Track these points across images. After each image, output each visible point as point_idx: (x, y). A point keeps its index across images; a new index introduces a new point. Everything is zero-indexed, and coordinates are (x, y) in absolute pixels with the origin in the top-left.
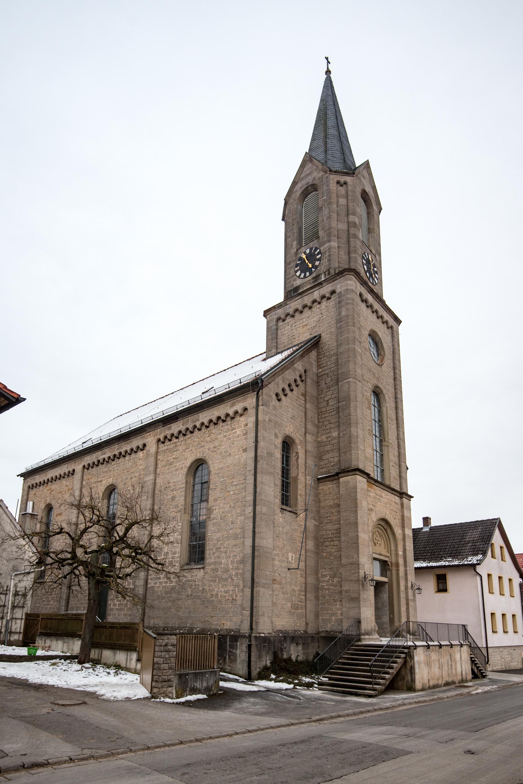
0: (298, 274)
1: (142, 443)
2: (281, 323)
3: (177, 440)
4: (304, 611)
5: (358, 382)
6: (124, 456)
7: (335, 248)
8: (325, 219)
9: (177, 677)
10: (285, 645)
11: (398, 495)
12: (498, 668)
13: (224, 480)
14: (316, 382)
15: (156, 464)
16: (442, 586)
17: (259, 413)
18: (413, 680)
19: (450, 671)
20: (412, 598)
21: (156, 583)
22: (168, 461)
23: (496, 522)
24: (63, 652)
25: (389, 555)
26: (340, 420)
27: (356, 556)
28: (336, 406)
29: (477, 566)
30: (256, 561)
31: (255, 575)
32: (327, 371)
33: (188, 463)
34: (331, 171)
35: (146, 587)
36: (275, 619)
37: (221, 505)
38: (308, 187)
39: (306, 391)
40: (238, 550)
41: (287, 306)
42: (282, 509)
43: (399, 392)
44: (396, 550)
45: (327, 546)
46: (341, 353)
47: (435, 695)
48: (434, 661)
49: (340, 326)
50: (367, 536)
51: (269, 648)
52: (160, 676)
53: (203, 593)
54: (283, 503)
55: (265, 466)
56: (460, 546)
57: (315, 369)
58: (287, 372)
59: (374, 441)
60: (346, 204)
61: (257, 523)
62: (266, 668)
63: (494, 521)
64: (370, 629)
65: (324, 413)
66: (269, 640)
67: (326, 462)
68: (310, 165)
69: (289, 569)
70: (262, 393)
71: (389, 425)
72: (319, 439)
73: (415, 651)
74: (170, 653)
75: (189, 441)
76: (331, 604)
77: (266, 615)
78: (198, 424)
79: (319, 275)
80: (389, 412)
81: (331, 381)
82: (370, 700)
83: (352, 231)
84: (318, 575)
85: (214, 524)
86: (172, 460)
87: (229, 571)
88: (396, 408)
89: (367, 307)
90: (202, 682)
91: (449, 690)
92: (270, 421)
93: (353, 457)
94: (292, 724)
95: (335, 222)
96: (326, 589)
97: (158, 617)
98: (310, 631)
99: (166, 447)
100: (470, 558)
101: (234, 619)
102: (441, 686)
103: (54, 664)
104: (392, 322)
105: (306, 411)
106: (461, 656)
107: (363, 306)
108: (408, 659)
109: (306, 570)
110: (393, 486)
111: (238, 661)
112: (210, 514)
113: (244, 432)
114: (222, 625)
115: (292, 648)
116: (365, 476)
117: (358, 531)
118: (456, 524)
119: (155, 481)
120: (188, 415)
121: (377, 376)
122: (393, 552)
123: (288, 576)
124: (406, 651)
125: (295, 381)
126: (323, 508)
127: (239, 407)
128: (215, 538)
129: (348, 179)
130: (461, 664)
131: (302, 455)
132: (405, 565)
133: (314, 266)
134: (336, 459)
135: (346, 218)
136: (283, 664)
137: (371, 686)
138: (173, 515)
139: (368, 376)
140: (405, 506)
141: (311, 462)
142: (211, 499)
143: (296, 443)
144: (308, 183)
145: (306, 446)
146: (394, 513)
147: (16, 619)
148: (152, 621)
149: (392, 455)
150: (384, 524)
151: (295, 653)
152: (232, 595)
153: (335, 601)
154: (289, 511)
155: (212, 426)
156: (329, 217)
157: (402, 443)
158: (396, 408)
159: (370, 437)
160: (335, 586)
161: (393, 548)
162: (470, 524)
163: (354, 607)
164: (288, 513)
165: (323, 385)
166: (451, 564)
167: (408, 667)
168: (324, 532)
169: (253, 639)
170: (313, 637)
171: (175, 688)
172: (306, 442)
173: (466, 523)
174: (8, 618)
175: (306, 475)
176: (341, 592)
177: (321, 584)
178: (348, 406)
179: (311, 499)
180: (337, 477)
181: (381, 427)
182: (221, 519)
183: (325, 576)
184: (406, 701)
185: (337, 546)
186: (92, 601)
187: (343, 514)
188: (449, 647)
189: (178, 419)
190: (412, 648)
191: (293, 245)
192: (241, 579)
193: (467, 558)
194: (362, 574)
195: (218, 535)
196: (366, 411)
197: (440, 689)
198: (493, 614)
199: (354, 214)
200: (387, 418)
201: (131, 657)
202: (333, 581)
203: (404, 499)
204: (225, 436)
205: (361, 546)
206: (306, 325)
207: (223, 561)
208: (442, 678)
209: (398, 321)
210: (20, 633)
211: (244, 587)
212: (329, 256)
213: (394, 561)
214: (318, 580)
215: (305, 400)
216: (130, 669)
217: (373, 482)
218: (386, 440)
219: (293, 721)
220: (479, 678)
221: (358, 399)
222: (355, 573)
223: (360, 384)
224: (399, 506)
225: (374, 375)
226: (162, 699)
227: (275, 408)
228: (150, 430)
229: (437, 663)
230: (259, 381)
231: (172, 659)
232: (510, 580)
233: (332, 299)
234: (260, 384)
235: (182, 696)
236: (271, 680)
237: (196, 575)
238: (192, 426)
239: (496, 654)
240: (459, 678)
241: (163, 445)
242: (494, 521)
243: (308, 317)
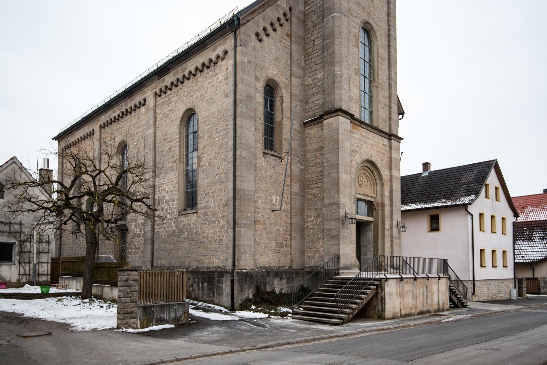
1: (143, 98)
3: (170, 92)
4: (289, 249)
5: (343, 16)
6: (130, 113)
9: (141, 310)
10: (268, 280)
11: (387, 137)
12: (485, 298)
14: (303, 21)
15: (155, 118)
16: (435, 227)
18: (383, 310)
19: (425, 301)
20: (397, 236)
21: (160, 228)
22: (164, 113)
23: (492, 164)
24: (77, 290)
25: (375, 196)
28: (321, 45)
29: (469, 206)
30: (237, 203)
31: (237, 217)
32: (313, 8)
35: (154, 232)
36: (258, 257)
39: (291, 31)
40: (223, 194)
42: (264, 153)
43: (392, 28)
44: (383, 191)
45: (312, 188)
47: (401, 323)
48: (408, 292)
50: (349, 176)
51: (251, 282)
53: (196, 235)
54: (266, 147)
55: (245, 110)
57: (301, 8)
58: (268, 9)
59: (362, 83)
61: (237, 167)
62: (248, 300)
63: (491, 163)
64: (349, 263)
65: (310, 54)
66: (252, 275)
70: (240, 32)
71: (380, 65)
72: (306, 82)
73: (386, 283)
74: (132, 288)
75: (180, 92)
77: (248, 253)
80: (380, 51)
82: (337, 328)
84: (304, 216)
85: (203, 171)
88: (389, 46)
90: (169, 313)
91: (420, 318)
92: (249, 62)
93: (336, 97)
94: (231, 352)
96: (310, 229)
98: (294, 267)
99: (162, 100)
100: (463, 199)
101: (221, 257)
102: (414, 315)
103: (59, 300)
105: (291, 52)
106: (438, 288)
108: (379, 290)
109: (291, 212)
110: (381, 127)
111: (224, 294)
115: (276, 282)
116: (349, 117)
117: (339, 172)
121: (367, 10)
122: (379, 193)
123: (272, 217)
124: (376, 283)
125: (279, 19)
126: (309, 152)
127: (219, 51)
128: (204, 184)
130: (438, 295)
132: (391, 205)
134: (321, 102)
137: (337, 315)
138: (171, 164)
139: (356, 10)
140: (393, 147)
142: (200, 147)
145: (291, 89)
146: (381, 155)
147: (42, 263)
148: (159, 261)
149: (382, 97)
150: (370, 166)
151: (279, 286)
152: (219, 236)
153: (318, 239)
154: (272, 155)
157: (393, 84)
158: (389, 46)
159: (357, 77)
160: (319, 226)
161: (379, 189)
164: (272, 157)
165: (310, 24)
167: (379, 297)
168: (310, 175)
169: (235, 275)
170: (297, 272)
171: (140, 319)
172: (291, 85)
173: (464, 166)
174: (35, 262)
176: (323, 231)
177: (306, 224)
178: (332, 43)
179: (295, 144)
180: (321, 120)
181: (371, 67)
183: (311, 217)
184: (384, 327)
185: (321, 187)
186: (89, 244)
187: (326, 156)
188: (426, 279)
189: (170, 70)
190: (383, 280)
193: (460, 199)
194: (342, 212)
196: (353, 49)
197: (412, 318)
198: (482, 251)
200: (378, 57)
204: (210, 83)
205: (341, 187)
207: (212, 205)
208: (416, 308)
210: (48, 275)
213: (379, 201)
214: (303, 220)
215: (291, 41)
217: (359, 123)
218: (376, 81)
219: (232, 349)
220: (459, 307)
221: (343, 36)
222: (336, 212)
223: (345, 19)
224: (387, 148)
225: (364, 10)
226: (125, 329)
227: (255, 49)
228: (149, 84)
229: (411, 294)
230: (235, 19)
231: (134, 293)
232: (503, 219)
234: (236, 22)
235: (148, 326)
237: (191, 220)
238: (181, 75)
239: (483, 286)
240: (436, 307)
242: (491, 163)
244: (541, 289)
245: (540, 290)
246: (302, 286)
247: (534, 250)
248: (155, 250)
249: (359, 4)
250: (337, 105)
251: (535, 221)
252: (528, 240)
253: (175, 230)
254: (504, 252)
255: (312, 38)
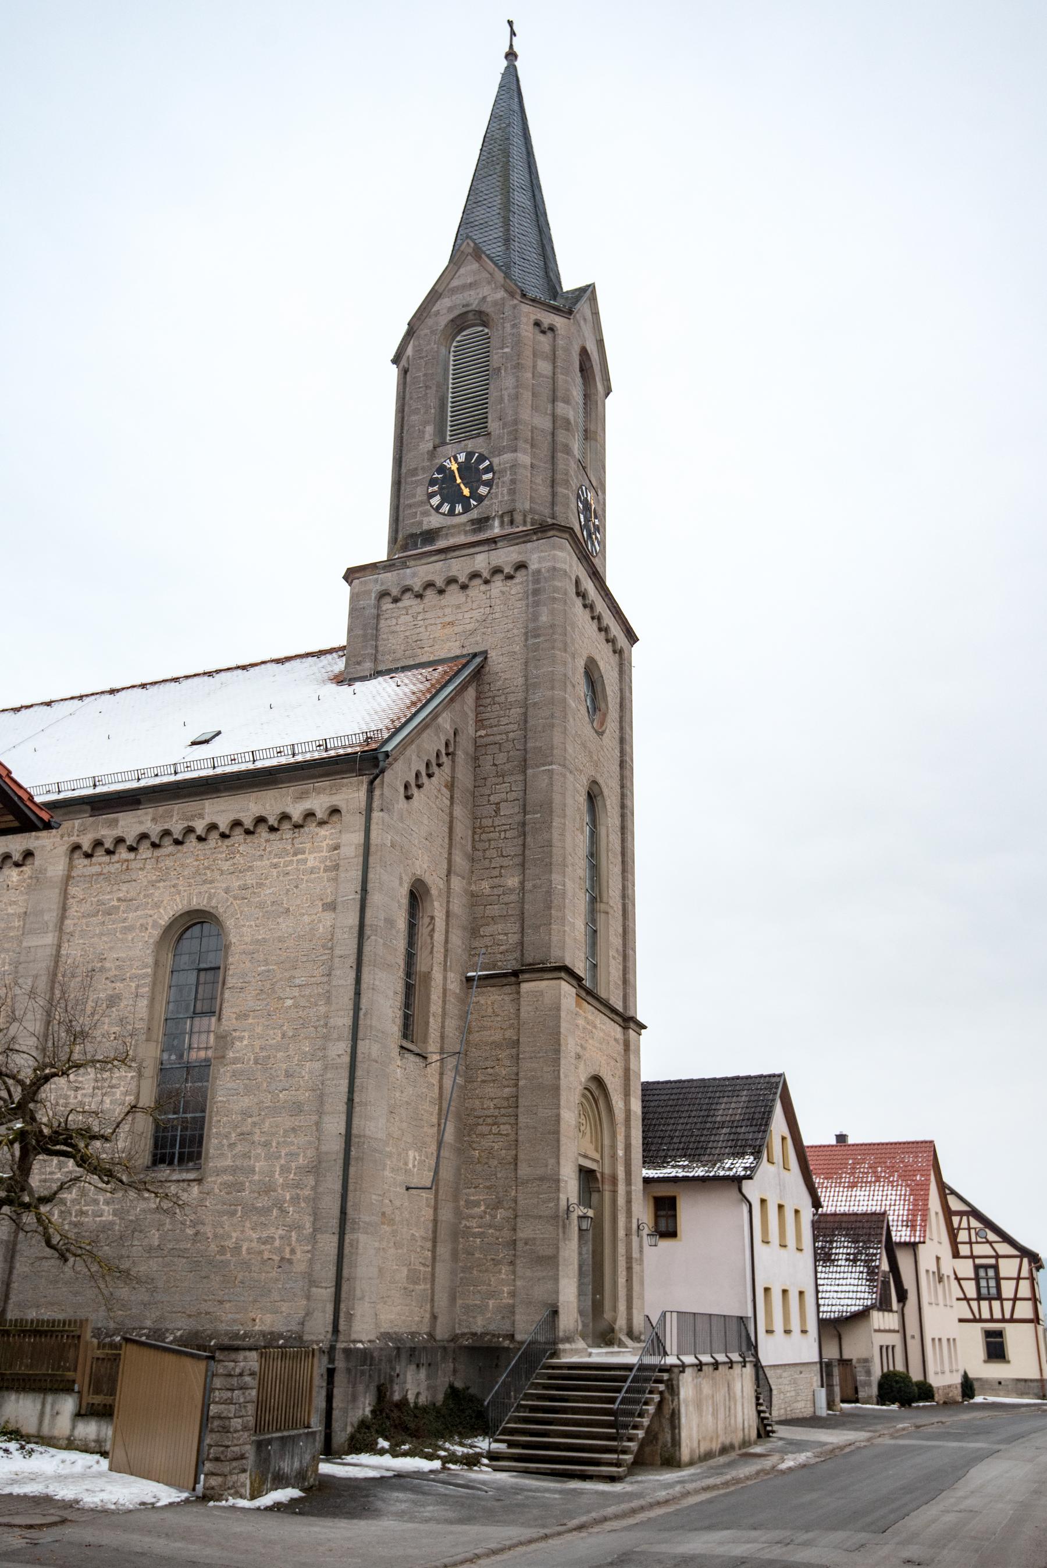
0: (436, 501)
2: (387, 605)
3: (132, 855)
4: (428, 1286)
7: (525, 467)
8: (506, 398)
11: (619, 1020)
13: (268, 971)
15: (64, 909)
17: (373, 827)
18: (676, 1442)
22: (101, 903)
23: (777, 1083)
25: (597, 1156)
26: (527, 852)
27: (552, 1161)
28: (518, 818)
29: (744, 1182)
31: (349, 1204)
33: (165, 917)
34: (524, 296)
37: (259, 1030)
38: (467, 312)
39: (453, 777)
40: (302, 1140)
41: (408, 570)
42: (402, 1047)
44: (613, 1147)
46: (535, 704)
49: (534, 644)
51: (370, 1376)
52: (227, 1447)
53: (195, 1241)
56: (705, 1132)
57: (471, 730)
60: (550, 374)
61: (358, 1082)
62: (363, 1425)
63: (773, 1080)
66: (372, 1358)
67: (487, 941)
68: (475, 266)
69: (408, 1189)
70: (383, 782)
71: (611, 866)
72: (473, 888)
75: (169, 862)
76: (486, 1271)
77: (367, 1299)
78: (200, 826)
79: (487, 519)
81: (508, 761)
82: (618, 1487)
83: (561, 436)
85: (234, 1074)
86: (115, 903)
87: (275, 1191)
89: (585, 606)
93: (554, 939)
95: (529, 411)
96: (475, 1235)
97: (52, 1304)
99: (96, 869)
104: (622, 641)
105: (451, 822)
107: (579, 602)
112: (225, 1048)
113: (328, 863)
114: (250, 1323)
115: (409, 1377)
116: (574, 983)
118: (692, 1081)
119: (58, 951)
120: (170, 799)
124: (666, 1376)
126: (477, 1046)
127: (319, 803)
129: (558, 321)
131: (440, 923)
133: (474, 494)
134: (514, 939)
135: (550, 406)
136: (396, 1414)
137: (615, 1456)
141: (457, 940)
142: (228, 1012)
143: (431, 895)
144: (467, 305)
146: (613, 1063)
151: (415, 1386)
152: (280, 1250)
153: (496, 1262)
155: (238, 835)
156: (517, 397)
161: (607, 1142)
162: (722, 1083)
163: (544, 1278)
165: (487, 767)
166: (691, 1175)
167: (667, 1412)
168: (477, 1102)
169: (339, 1356)
170: (445, 1348)
173: (714, 1079)
175: (445, 970)
177: (464, 1222)
178: (547, 825)
180: (513, 979)
182: (256, 1063)
183: (477, 1204)
185: (507, 1135)
187: (525, 1065)
190: (676, 1370)
191: (424, 432)
192: (309, 1210)
195: (246, 1102)
198: (767, 1290)
199: (567, 401)
201: (57, 1407)
202: (494, 1217)
203: (631, 1031)
204: (275, 866)
206: (451, 624)
208: (717, 1437)
209: (632, 638)
211: (315, 1230)
212: (513, 482)
215: (452, 797)
216: (51, 1438)
218: (605, 899)
221: (568, 812)
222: (549, 1200)
224: (620, 1048)
225: (591, 757)
232: (797, 1212)
233: (516, 581)
236: (382, 1452)
241: (86, 862)
242: (773, 1080)
243: (458, 607)
244: (860, 1389)
245: (856, 1392)
246: (451, 1387)
247: (840, 1288)
248: (14, 1277)
249: (585, 747)
250: (555, 957)
251: (835, 1215)
252: (825, 1261)
253: (112, 1223)
254: (801, 1293)
255: (492, 798)
